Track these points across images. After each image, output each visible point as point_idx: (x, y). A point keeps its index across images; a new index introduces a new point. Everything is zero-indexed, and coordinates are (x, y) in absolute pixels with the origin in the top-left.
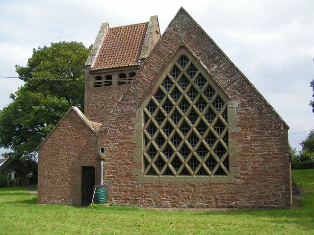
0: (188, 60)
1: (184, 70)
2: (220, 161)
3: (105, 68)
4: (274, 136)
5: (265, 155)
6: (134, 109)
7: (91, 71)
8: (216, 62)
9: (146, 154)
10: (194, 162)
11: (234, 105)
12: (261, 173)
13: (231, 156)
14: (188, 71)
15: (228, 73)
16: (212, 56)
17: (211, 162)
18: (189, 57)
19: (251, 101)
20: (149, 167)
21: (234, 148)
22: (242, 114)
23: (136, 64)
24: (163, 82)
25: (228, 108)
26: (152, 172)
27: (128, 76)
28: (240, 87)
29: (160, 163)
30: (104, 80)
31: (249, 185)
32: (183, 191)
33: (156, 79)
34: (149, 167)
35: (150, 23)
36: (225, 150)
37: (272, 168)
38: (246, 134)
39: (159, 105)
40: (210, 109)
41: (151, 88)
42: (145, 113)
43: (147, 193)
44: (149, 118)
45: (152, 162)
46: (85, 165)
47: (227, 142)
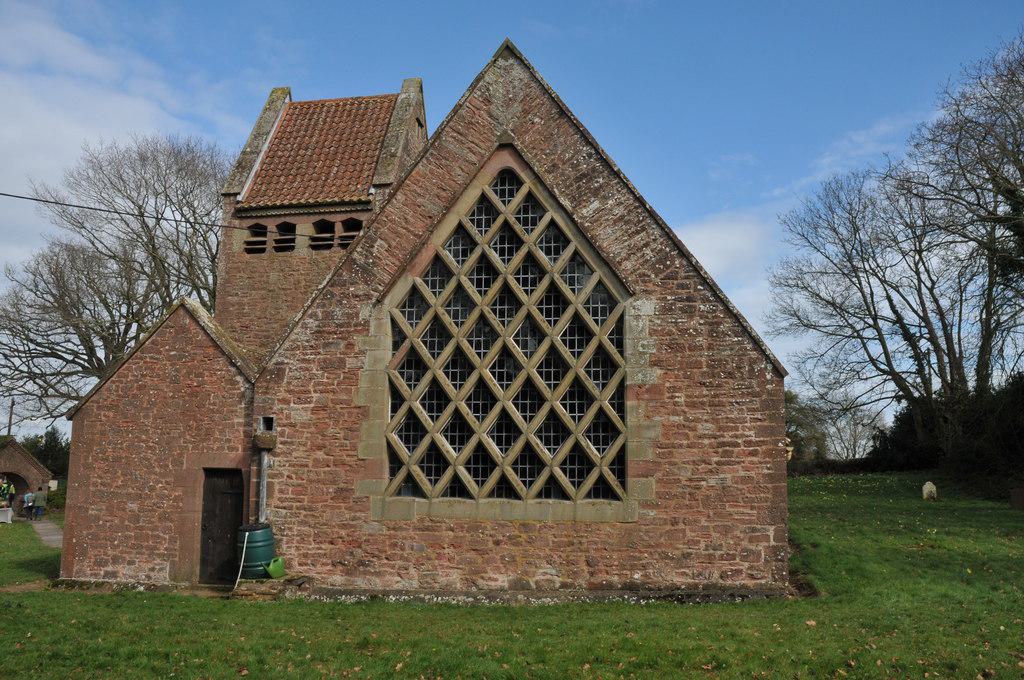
0: (520, 183)
1: (508, 210)
2: (602, 459)
3: (278, 203)
4: (749, 394)
5: (723, 444)
6: (365, 312)
7: (238, 211)
8: (596, 193)
9: (395, 438)
10: (481, 463)
11: (642, 311)
12: (712, 493)
13: (631, 446)
14: (519, 212)
15: (626, 223)
16: (584, 176)
17: (578, 463)
18: (523, 175)
19: (689, 299)
20: (401, 475)
21: (640, 428)
22: (663, 333)
23: (363, 198)
24: (449, 238)
25: (627, 317)
26: (411, 487)
27: (339, 230)
28: (660, 261)
29: (435, 462)
30: (272, 236)
31: (681, 526)
32: (497, 543)
33: (432, 229)
34: (401, 475)
35: (403, 96)
36: (616, 432)
37: (745, 480)
38: (674, 389)
39: (437, 301)
40: (459, 350)
41: (414, 254)
42: (393, 322)
43: (394, 545)
44: (404, 338)
45: (411, 458)
46: (215, 465)
47: (621, 409)
